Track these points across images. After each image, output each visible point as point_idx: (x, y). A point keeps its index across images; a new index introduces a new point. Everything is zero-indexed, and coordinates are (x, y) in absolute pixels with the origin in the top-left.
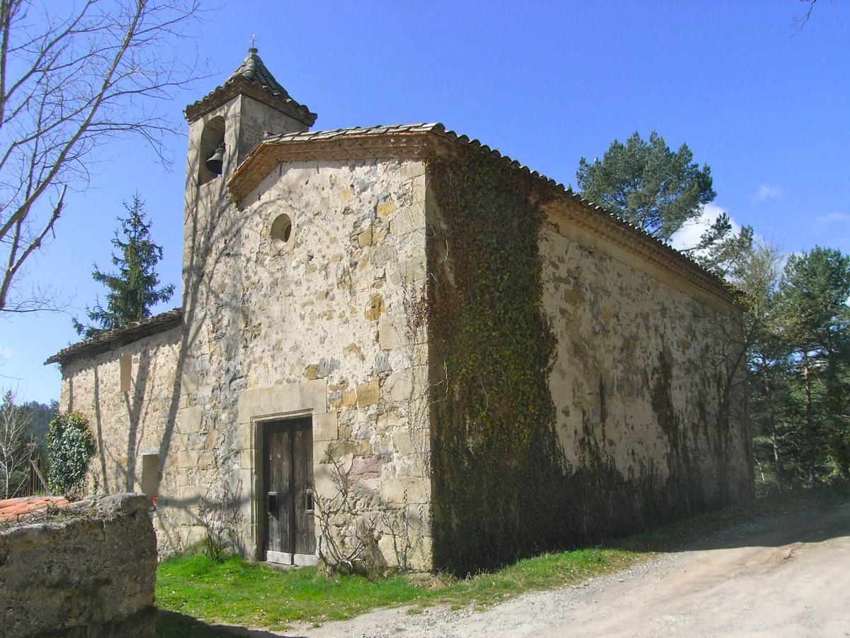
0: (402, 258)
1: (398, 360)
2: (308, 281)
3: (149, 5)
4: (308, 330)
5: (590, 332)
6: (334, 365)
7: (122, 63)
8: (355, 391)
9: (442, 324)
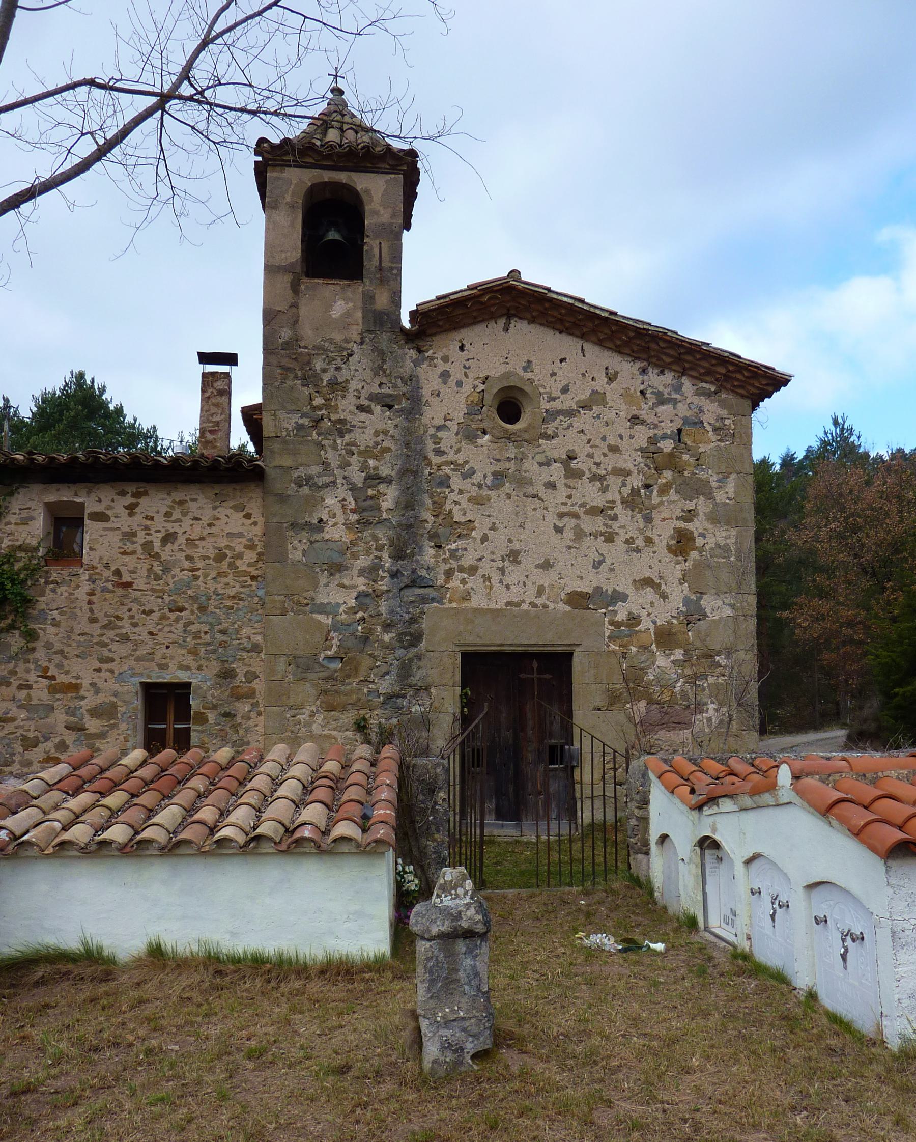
0: (720, 497)
1: (717, 608)
2: (568, 486)
3: (69, 3)
4: (569, 548)
5: (424, 573)
6: (618, 597)
7: (195, 730)
8: (652, 631)
9: (454, 564)
